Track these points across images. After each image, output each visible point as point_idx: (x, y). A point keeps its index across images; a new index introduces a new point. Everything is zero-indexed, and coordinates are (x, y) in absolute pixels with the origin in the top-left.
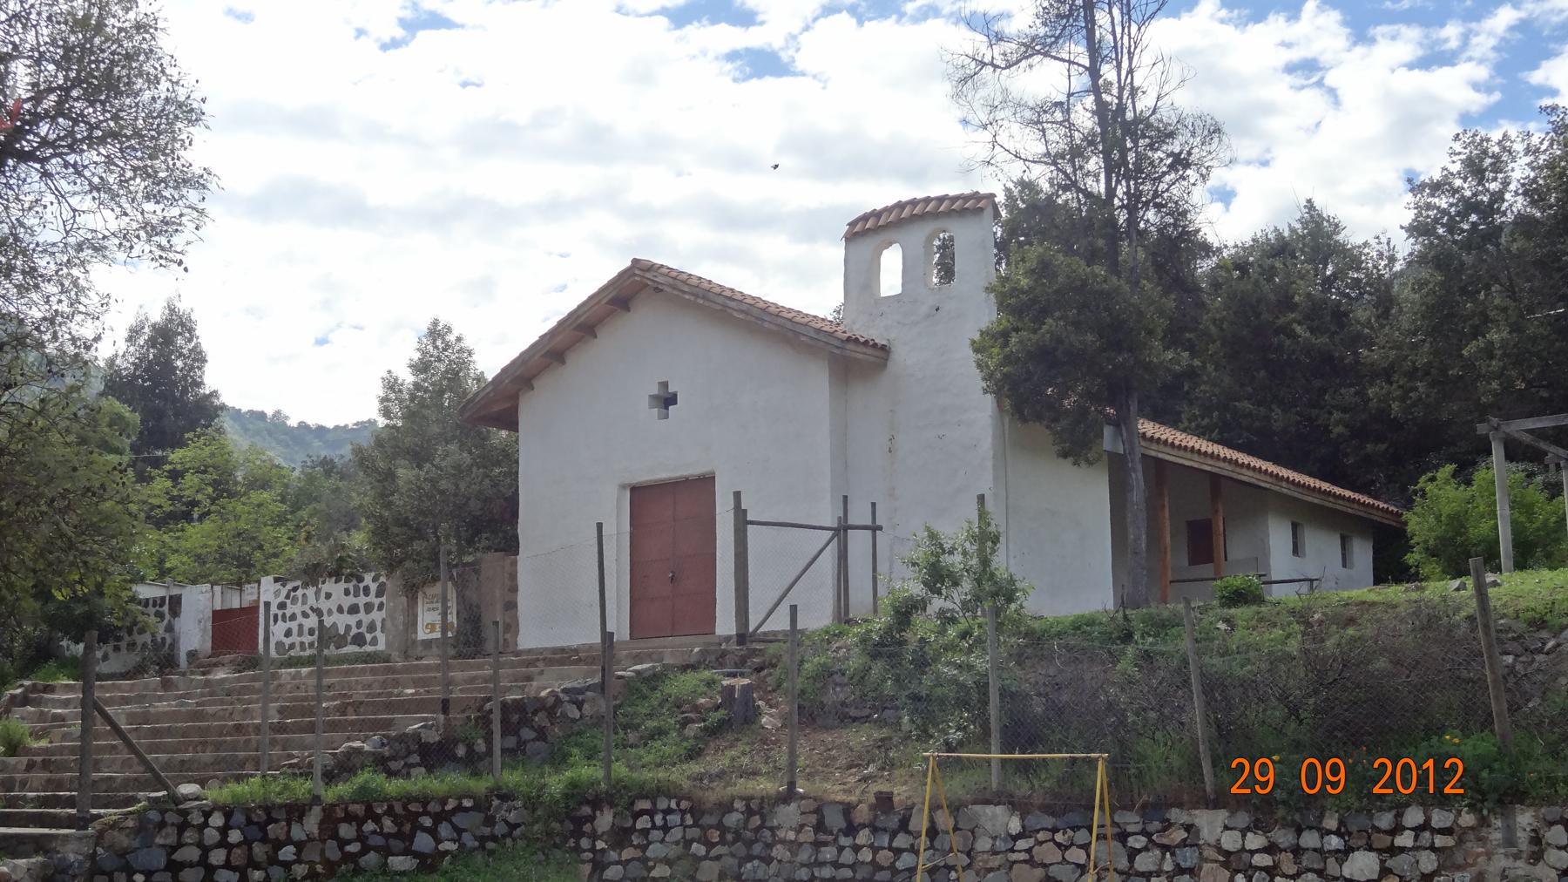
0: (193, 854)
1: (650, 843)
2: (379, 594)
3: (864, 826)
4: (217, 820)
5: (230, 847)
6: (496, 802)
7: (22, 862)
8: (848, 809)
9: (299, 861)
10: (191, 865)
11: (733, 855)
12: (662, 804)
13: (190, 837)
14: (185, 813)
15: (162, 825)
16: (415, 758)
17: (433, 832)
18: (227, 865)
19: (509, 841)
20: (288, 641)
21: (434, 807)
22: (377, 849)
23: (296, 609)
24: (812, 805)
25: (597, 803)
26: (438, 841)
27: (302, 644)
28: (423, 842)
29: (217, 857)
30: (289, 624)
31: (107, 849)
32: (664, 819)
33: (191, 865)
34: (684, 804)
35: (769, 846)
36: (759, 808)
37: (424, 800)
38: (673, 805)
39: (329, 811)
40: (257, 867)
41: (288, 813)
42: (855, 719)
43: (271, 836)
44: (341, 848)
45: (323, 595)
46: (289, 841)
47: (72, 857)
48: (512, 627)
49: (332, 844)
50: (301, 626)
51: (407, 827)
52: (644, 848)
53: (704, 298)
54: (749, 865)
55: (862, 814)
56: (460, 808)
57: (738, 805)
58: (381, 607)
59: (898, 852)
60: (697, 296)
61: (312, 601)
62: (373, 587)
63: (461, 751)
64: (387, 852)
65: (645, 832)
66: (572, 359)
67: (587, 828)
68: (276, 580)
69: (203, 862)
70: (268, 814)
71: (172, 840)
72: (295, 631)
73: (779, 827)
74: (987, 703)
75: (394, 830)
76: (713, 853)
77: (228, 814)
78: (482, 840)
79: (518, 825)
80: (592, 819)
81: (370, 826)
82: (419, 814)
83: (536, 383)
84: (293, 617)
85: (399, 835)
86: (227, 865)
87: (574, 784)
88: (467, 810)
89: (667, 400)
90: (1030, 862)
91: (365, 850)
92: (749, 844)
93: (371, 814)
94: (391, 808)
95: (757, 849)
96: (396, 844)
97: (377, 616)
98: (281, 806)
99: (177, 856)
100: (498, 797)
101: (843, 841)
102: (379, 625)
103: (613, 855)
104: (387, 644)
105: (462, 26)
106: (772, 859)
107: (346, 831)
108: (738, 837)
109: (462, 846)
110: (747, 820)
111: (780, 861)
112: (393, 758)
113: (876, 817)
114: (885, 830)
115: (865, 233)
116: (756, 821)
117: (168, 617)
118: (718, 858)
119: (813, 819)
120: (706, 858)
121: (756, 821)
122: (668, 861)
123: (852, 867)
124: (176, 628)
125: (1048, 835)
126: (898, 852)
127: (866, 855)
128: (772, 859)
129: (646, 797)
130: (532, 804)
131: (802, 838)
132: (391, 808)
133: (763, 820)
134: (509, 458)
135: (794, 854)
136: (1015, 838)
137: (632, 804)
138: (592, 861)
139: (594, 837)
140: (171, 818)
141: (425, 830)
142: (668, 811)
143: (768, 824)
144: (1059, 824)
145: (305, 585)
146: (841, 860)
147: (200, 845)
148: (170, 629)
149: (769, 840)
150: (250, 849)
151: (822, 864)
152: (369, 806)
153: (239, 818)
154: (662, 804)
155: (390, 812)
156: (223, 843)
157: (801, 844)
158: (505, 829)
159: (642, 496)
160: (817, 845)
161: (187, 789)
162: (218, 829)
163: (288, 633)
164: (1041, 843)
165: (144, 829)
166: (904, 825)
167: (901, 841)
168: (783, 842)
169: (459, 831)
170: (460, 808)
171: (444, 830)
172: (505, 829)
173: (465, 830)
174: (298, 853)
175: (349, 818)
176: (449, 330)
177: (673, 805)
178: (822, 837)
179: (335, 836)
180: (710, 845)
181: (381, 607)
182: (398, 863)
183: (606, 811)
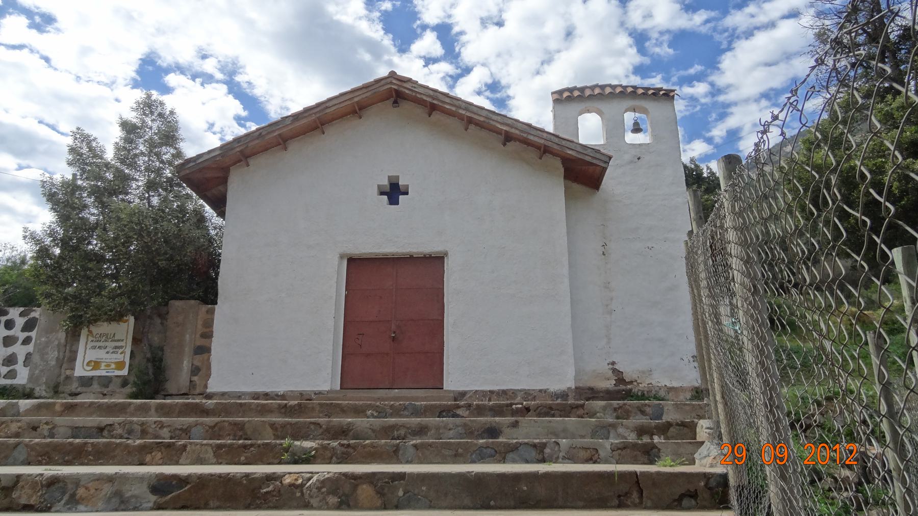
48: (201, 370)
58: (27, 341)
62: (20, 322)
66: (293, 146)
74: (75, 359)
83: (251, 161)
102: (21, 359)
104: (31, 378)
105: (56, 69)
115: (570, 99)
176: (202, 84)
181: (27, 341)
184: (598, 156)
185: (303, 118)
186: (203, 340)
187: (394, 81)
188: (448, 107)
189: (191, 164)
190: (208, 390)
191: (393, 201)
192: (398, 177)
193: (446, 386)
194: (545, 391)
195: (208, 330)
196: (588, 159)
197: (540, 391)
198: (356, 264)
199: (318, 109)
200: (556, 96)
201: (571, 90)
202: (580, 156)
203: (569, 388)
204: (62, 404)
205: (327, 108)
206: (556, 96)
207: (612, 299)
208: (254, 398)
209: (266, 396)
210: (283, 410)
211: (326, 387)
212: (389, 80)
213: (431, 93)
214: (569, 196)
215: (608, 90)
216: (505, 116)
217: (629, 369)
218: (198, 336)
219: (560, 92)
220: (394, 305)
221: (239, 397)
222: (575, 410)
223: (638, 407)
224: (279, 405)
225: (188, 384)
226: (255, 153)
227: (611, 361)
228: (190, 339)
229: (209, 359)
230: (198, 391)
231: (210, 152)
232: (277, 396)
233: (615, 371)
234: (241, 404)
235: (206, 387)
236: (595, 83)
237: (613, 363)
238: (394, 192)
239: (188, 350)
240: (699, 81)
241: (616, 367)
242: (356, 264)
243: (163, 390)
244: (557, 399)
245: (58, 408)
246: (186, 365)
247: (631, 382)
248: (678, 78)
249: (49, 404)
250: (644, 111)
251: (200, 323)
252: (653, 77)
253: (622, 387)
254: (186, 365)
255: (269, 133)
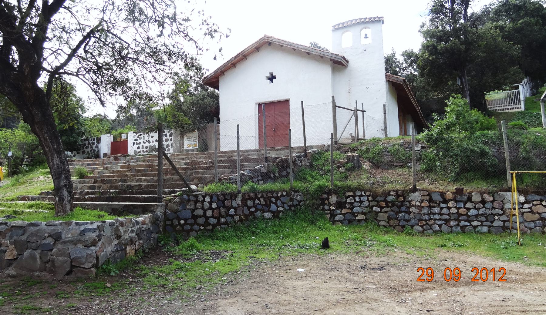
0: (200, 212)
1: (354, 207)
2: (171, 136)
3: (451, 200)
4: (208, 199)
5: (213, 209)
6: (293, 193)
7: (146, 215)
8: (442, 194)
9: (236, 215)
10: (200, 217)
11: (392, 211)
12: (358, 193)
13: (199, 205)
14: (196, 196)
15: (189, 201)
16: (260, 178)
17: (276, 203)
18: (213, 216)
19: (298, 207)
20: (138, 150)
21: (275, 195)
22: (260, 210)
23: (142, 141)
24: (426, 193)
25: (330, 193)
26: (278, 207)
27: (143, 151)
28: (273, 207)
29: (209, 213)
30: (138, 145)
31: (170, 210)
32: (360, 198)
33: (200, 217)
34: (368, 193)
35: (409, 208)
36: (403, 194)
37: (272, 192)
38: (363, 193)
39: (244, 195)
40: (223, 217)
41: (231, 196)
42: (397, 166)
43: (226, 205)
44: (249, 210)
45: (150, 137)
46: (232, 207)
47: (159, 214)
49: (245, 208)
50: (143, 146)
51: (268, 202)
52: (352, 209)
53: (291, 45)
54: (400, 215)
55: (449, 195)
56: (282, 195)
57: (392, 193)
58: (171, 140)
59: (469, 209)
60: (288, 45)
61: (146, 138)
62: (168, 134)
63: (272, 176)
64: (263, 211)
65: (351, 203)
66: (238, 66)
67: (326, 202)
68: (134, 132)
69: (204, 215)
70: (225, 197)
71: (193, 207)
72: (141, 148)
73: (412, 201)
75: (264, 203)
76: (383, 210)
77: (211, 197)
78: (290, 206)
79: (302, 201)
80: (328, 199)
81: (257, 202)
82: (271, 197)
83: (225, 73)
84: (140, 143)
85: (265, 205)
86: (213, 216)
87: (320, 187)
88: (284, 196)
89: (272, 78)
90: (532, 212)
91: (256, 210)
92: (399, 207)
93: (257, 198)
94: (262, 194)
95: (403, 209)
96: (266, 208)
97: (170, 143)
98: (229, 194)
99: (196, 213)
100: (294, 191)
101: (442, 205)
103: (338, 212)
104: (174, 151)
106: (411, 212)
107: (250, 203)
108: (394, 204)
109: (285, 209)
110: (397, 198)
111: (414, 213)
112: (254, 177)
113: (456, 197)
114: (461, 201)
116: (402, 199)
117: (96, 143)
118: (386, 212)
119: (427, 198)
120: (380, 212)
121: (402, 199)
122: (363, 213)
123: (448, 215)
124: (99, 147)
125: (539, 202)
126: (469, 209)
127: (454, 211)
128: (411, 212)
129: (351, 191)
130: (306, 193)
131: (423, 205)
132: (262, 194)
133: (404, 198)
134: (216, 98)
135: (420, 210)
136: (523, 204)
137: (345, 193)
138: (330, 213)
139: (329, 205)
140: (192, 198)
141: (274, 203)
142: (361, 196)
143: (406, 200)
144: (543, 198)
145: (144, 133)
146: (442, 212)
147: (202, 208)
148: (97, 147)
149: (408, 205)
150: (220, 210)
151: (434, 214)
152: (253, 195)
153: (215, 198)
154: (358, 193)
155: (262, 196)
156: (210, 208)
157: (423, 207)
158: (297, 203)
159: (263, 107)
160: (430, 207)
161: (194, 187)
162: (208, 202)
163: (138, 148)
164: (535, 205)
165: (183, 203)
166: (470, 199)
167: (469, 205)
168: (415, 206)
169: (283, 203)
170: (282, 195)
171: (279, 203)
172: (297, 203)
173: (285, 203)
174: (235, 212)
175: (250, 198)
177: (363, 193)
178: (432, 204)
179: (246, 205)
180: (381, 208)
181: (171, 140)
182: (267, 215)
183: (333, 196)
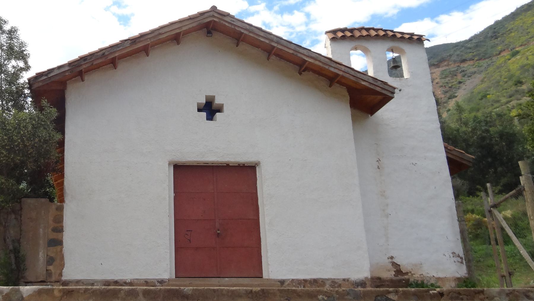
48: (56, 260)
66: (122, 66)
115: (344, 37)
184: (386, 87)
185: (139, 42)
186: (55, 234)
187: (216, 15)
188: (262, 39)
189: (44, 78)
190: (64, 278)
191: (211, 116)
192: (214, 96)
193: (265, 276)
194: (348, 280)
195: (58, 225)
196: (378, 89)
197: (344, 280)
198: (181, 170)
199: (152, 35)
200: (332, 36)
201: (343, 30)
202: (372, 87)
203: (366, 278)
204: (60, 291)
205: (160, 34)
206: (332, 36)
207: (387, 205)
208: (105, 285)
209: (116, 283)
210: (250, 295)
211: (166, 276)
212: (211, 13)
213: (248, 27)
214: (355, 120)
215: (373, 33)
216: (310, 50)
217: (406, 261)
218: (50, 230)
219: (334, 32)
220: (216, 205)
221: (93, 284)
222: (478, 295)
223: (524, 293)
224: (246, 291)
225: (45, 272)
226: (89, 70)
227: (390, 255)
228: (44, 233)
229: (61, 250)
230: (53, 279)
231: (59, 67)
232: (126, 283)
233: (394, 264)
234: (214, 290)
235: (61, 275)
236: (371, 26)
237: (392, 258)
238: (210, 109)
239: (42, 242)
240: (298, 10)
241: (395, 260)
242: (181, 170)
243: (23, 277)
244: (358, 286)
245: (56, 293)
246: (42, 256)
247: (407, 273)
248: (280, 7)
249: (49, 290)
250: (401, 51)
251: (51, 218)
252: (259, 4)
253: (400, 277)
254: (42, 256)
255: (111, 53)
